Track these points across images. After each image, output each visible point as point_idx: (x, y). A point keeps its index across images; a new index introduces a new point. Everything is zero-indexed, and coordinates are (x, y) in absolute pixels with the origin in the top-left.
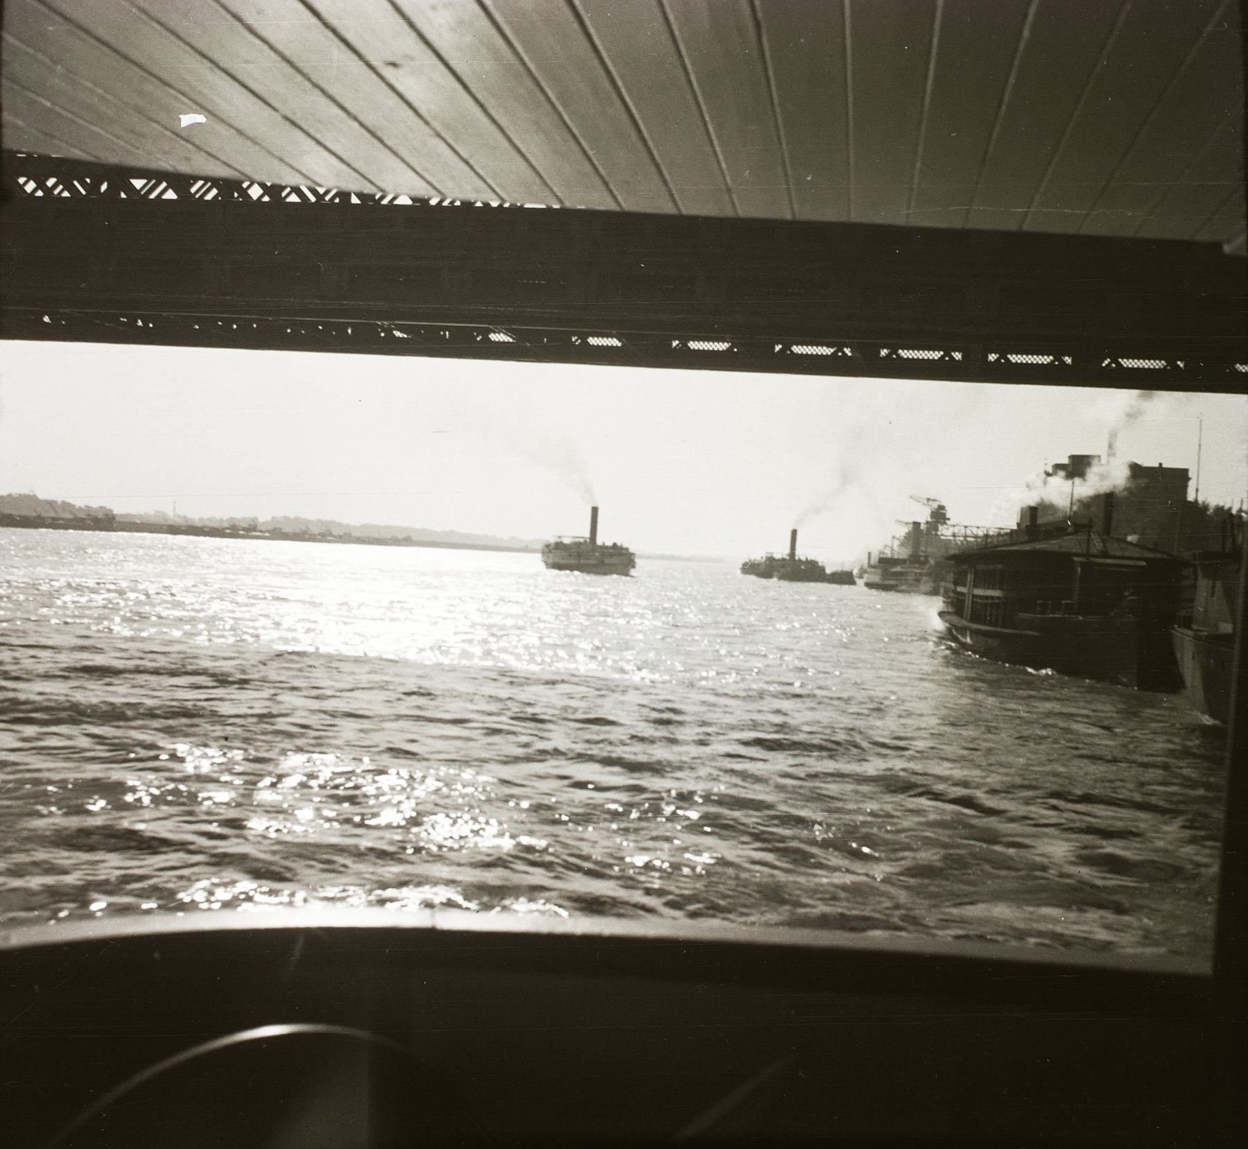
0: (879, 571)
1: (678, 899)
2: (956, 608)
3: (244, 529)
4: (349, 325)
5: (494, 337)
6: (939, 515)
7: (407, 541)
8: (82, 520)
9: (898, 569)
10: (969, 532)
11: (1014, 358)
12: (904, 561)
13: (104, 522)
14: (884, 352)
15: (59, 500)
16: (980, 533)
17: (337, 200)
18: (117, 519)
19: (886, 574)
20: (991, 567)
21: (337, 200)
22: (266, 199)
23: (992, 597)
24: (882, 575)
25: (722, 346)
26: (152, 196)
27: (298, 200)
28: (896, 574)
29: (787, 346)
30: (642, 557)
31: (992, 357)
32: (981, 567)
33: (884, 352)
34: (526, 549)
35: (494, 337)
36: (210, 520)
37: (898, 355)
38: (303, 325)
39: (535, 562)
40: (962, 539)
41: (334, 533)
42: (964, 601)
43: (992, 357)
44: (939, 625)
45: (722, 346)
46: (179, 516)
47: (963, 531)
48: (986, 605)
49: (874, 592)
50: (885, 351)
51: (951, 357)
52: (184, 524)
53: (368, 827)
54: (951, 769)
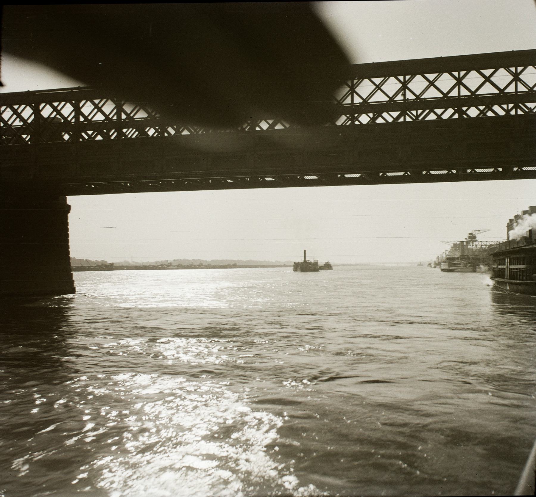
0: (447, 264)
1: (94, 438)
2: (497, 274)
3: (166, 265)
4: (210, 179)
5: (268, 179)
6: (472, 237)
7: (234, 266)
8: (100, 266)
9: (456, 262)
10: (482, 244)
11: (478, 171)
12: (458, 258)
13: (110, 267)
14: (424, 173)
15: (85, 259)
16: (488, 244)
17: (166, 135)
18: (114, 265)
19: (450, 265)
20: (518, 256)
21: (166, 135)
22: (464, 109)
23: (520, 269)
24: (449, 265)
25: (358, 175)
26: (428, 111)
27: (189, 133)
28: (455, 264)
29: (384, 173)
30: (335, 266)
31: (469, 171)
32: (512, 256)
33: (424, 173)
34: (285, 266)
35: (268, 179)
36: (148, 262)
37: (430, 173)
38: (192, 181)
39: (290, 270)
40: (480, 247)
41: (204, 264)
42: (505, 271)
43: (469, 171)
44: (491, 283)
45: (358, 175)
46: (134, 262)
47: (480, 243)
48: (517, 271)
49: (445, 273)
50: (425, 172)
51: (452, 172)
52: (142, 265)
53: (208, 386)
54: (518, 343)
